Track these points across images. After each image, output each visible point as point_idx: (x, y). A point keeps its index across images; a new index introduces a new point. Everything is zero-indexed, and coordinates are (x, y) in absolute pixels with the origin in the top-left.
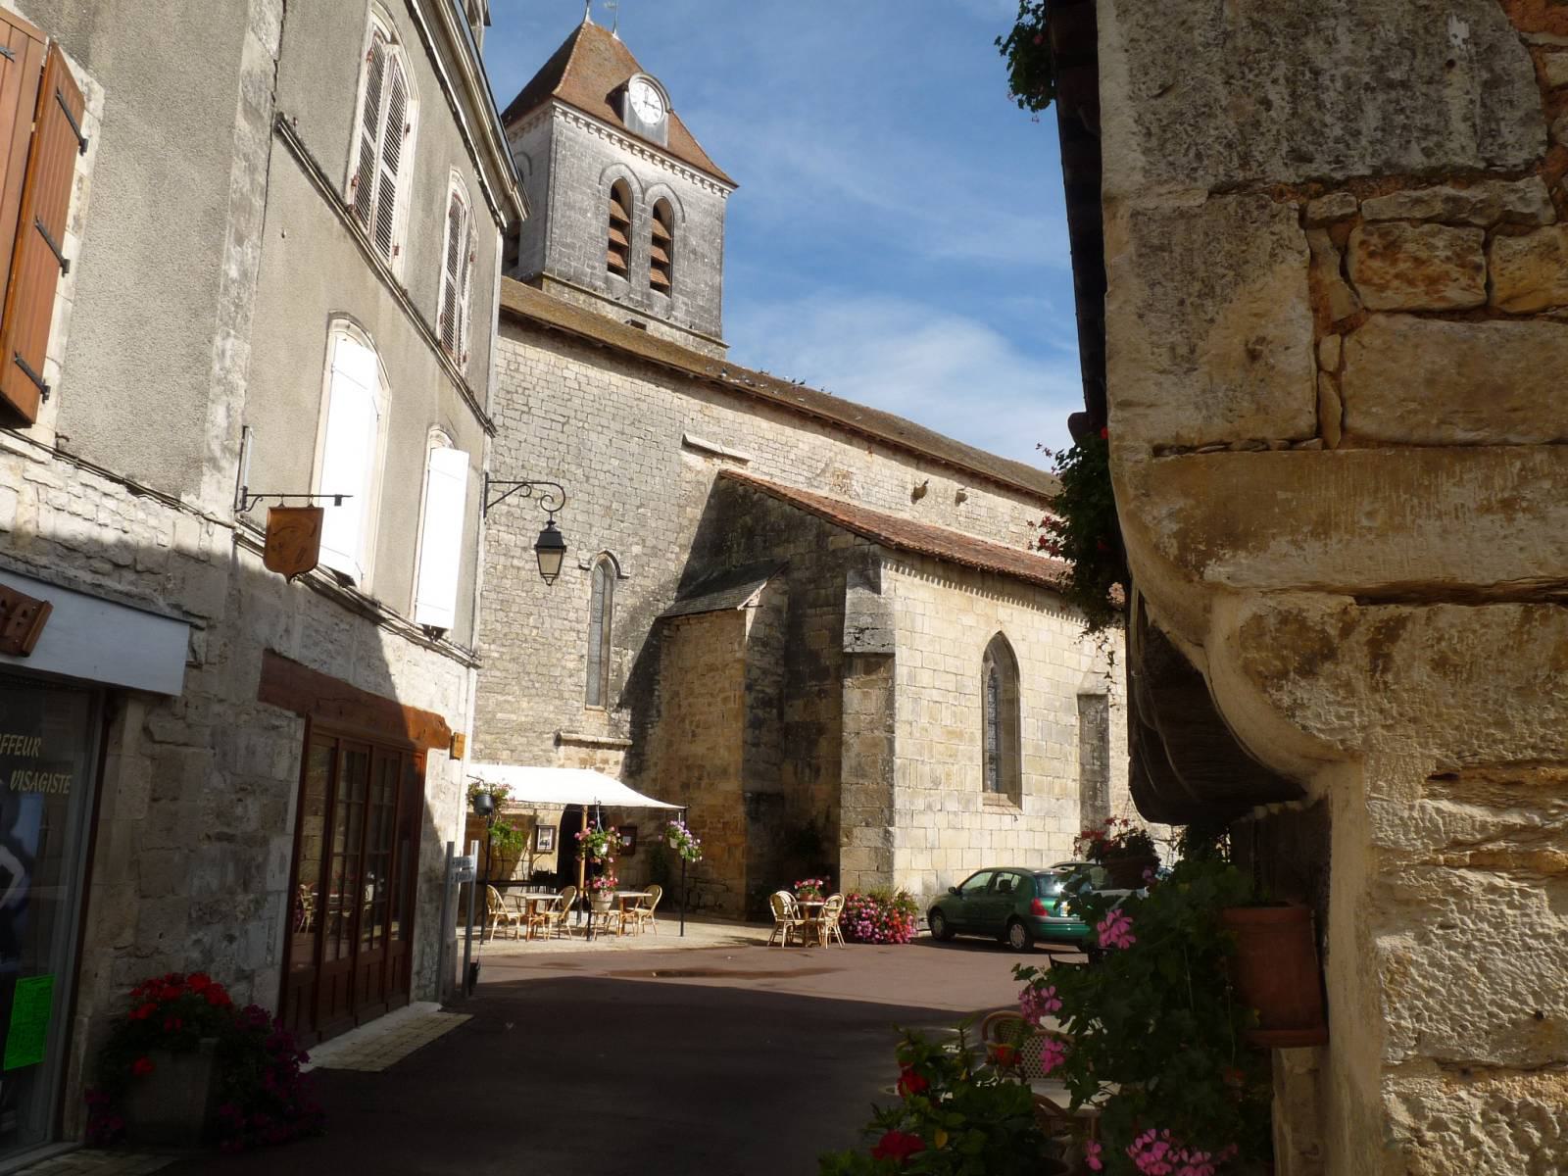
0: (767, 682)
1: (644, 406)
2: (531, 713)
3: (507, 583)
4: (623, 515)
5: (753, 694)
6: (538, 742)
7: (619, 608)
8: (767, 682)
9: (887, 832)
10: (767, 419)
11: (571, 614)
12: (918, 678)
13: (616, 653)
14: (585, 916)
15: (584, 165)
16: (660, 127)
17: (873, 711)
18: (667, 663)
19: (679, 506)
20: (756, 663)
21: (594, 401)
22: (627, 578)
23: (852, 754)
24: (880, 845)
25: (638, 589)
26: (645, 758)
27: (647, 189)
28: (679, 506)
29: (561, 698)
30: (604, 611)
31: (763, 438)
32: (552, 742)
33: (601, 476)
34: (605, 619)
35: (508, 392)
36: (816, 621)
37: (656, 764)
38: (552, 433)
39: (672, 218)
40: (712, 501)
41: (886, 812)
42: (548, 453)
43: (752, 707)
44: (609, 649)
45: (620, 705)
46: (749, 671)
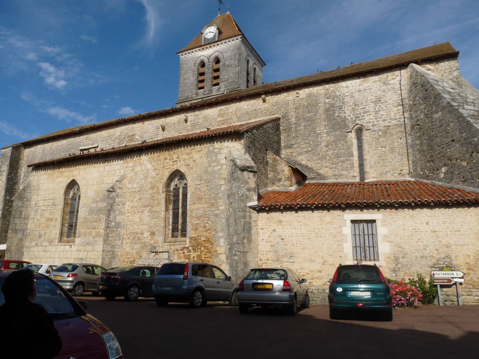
12: (38, 204)
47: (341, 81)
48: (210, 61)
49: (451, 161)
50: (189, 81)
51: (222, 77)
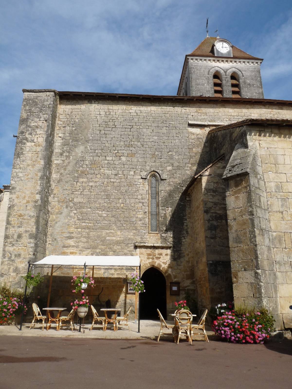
0: (217, 208)
1: (168, 115)
2: (122, 236)
3: (109, 188)
4: (161, 156)
5: (209, 215)
6: (126, 247)
7: (163, 192)
8: (217, 208)
9: (256, 273)
10: (232, 108)
11: (139, 196)
12: (285, 188)
13: (162, 209)
15: (201, 71)
16: (229, 52)
17: (241, 205)
18: (189, 211)
19: (189, 149)
20: (210, 200)
21: (144, 118)
22: (166, 179)
23: (233, 231)
24: (253, 281)
25: (172, 183)
26: (182, 252)
27: (227, 71)
28: (189, 149)
29: (136, 229)
30: (155, 194)
31: (231, 116)
32: (133, 247)
33: (149, 144)
34: (157, 197)
35: (106, 122)
37: (188, 255)
38: (126, 133)
40: (207, 144)
41: (254, 261)
42: (124, 140)
43: (209, 221)
44: (159, 208)
45: (167, 231)
46: (206, 204)
47: (87, 102)
48: (227, 74)
49: (83, 161)
50: (204, 87)
51: (244, 93)
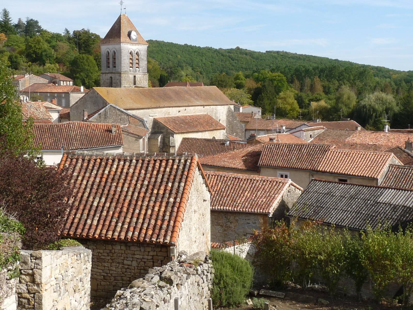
14: (80, 159)
36: (166, 140)
39: (139, 54)
